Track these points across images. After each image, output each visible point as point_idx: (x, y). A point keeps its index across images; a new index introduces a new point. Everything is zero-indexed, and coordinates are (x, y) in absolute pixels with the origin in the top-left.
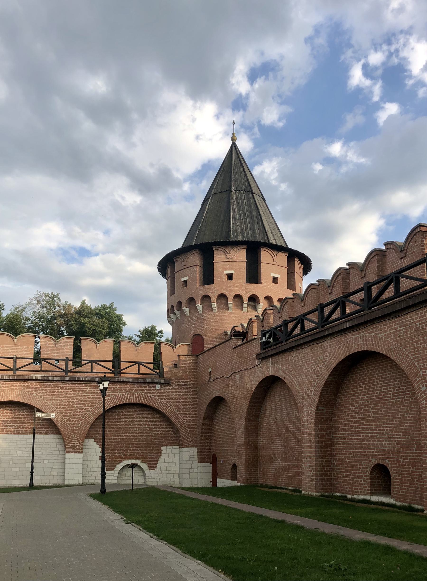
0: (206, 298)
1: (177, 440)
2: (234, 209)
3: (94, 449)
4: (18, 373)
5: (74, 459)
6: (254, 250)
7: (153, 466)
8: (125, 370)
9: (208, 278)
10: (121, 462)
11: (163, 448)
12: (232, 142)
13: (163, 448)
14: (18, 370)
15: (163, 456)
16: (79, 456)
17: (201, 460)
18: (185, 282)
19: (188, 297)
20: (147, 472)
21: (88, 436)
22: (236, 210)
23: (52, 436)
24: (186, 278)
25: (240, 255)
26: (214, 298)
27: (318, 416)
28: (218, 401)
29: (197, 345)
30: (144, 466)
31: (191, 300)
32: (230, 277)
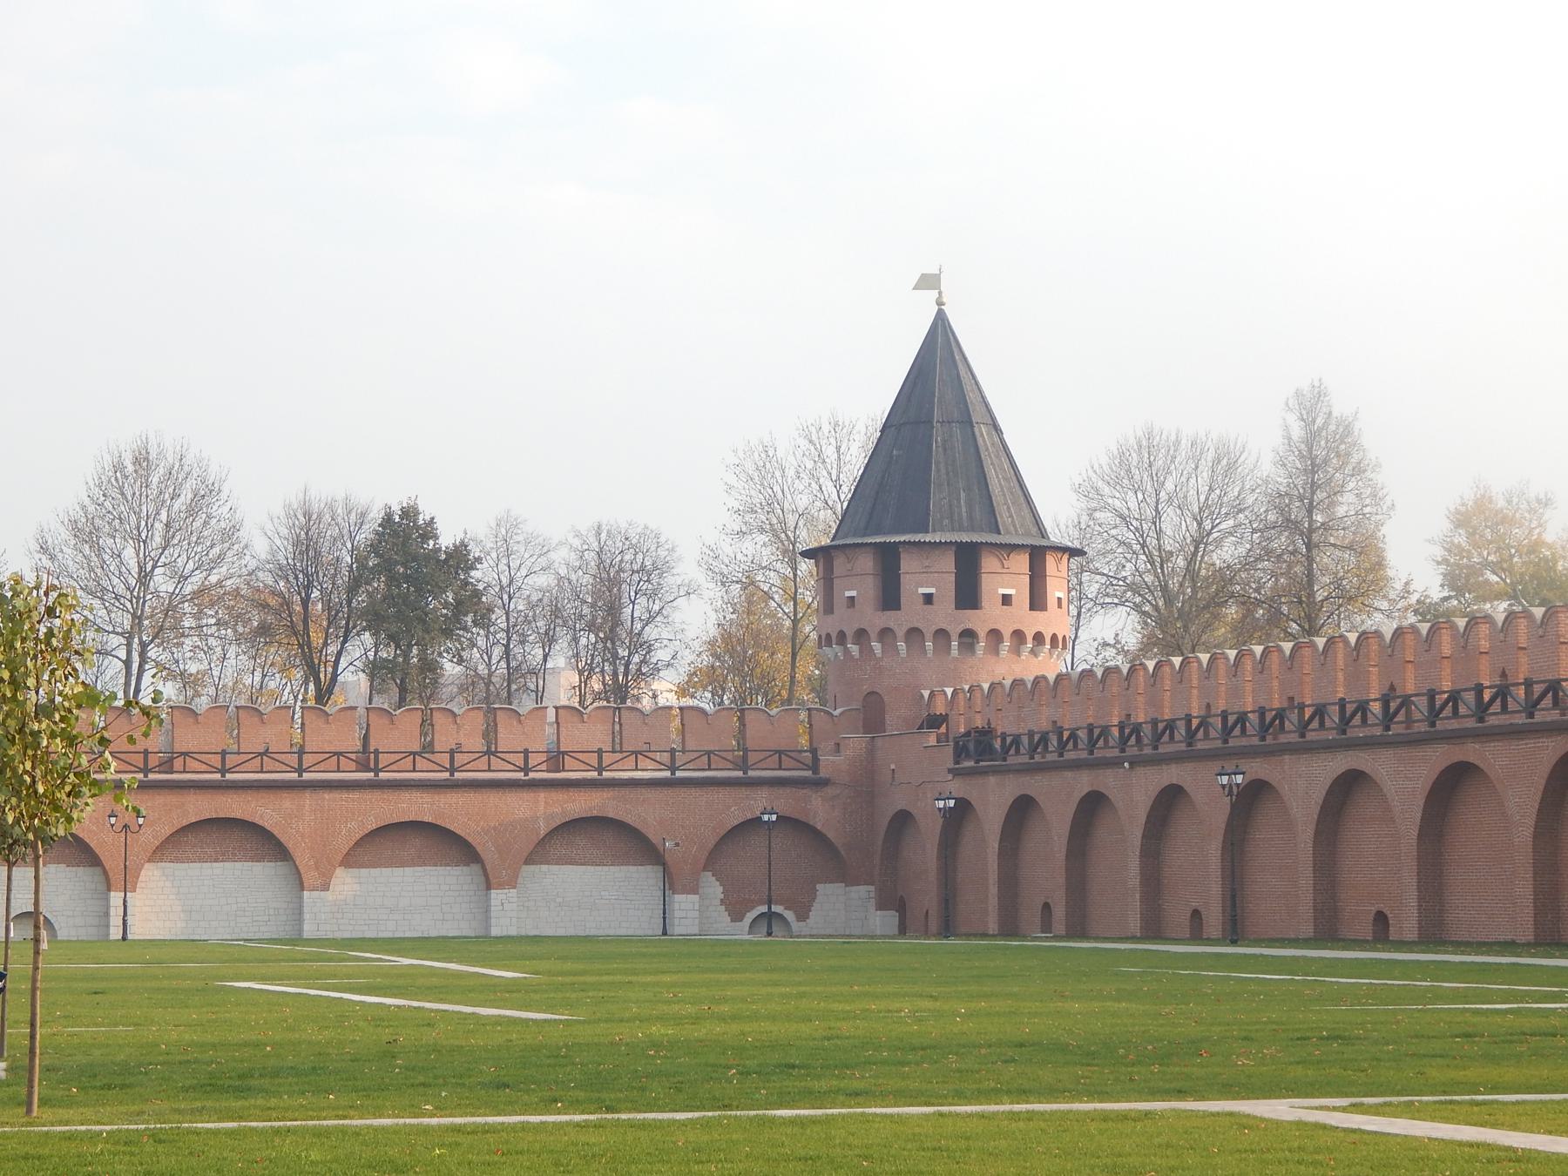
0: (968, 635)
1: (844, 874)
2: (937, 463)
3: (713, 889)
4: (228, 776)
5: (684, 904)
6: (1038, 555)
7: (803, 916)
8: (287, 802)
9: (890, 598)
10: (752, 908)
11: (818, 886)
12: (936, 308)
13: (818, 886)
14: (229, 771)
15: (819, 898)
16: (695, 898)
17: (881, 906)
18: (852, 598)
19: (856, 626)
20: (796, 926)
21: (705, 869)
22: (942, 466)
23: (633, 870)
24: (853, 593)
25: (1021, 562)
26: (900, 633)
27: (1001, 854)
28: (903, 820)
29: (872, 715)
30: (789, 915)
31: (861, 635)
32: (928, 599)
